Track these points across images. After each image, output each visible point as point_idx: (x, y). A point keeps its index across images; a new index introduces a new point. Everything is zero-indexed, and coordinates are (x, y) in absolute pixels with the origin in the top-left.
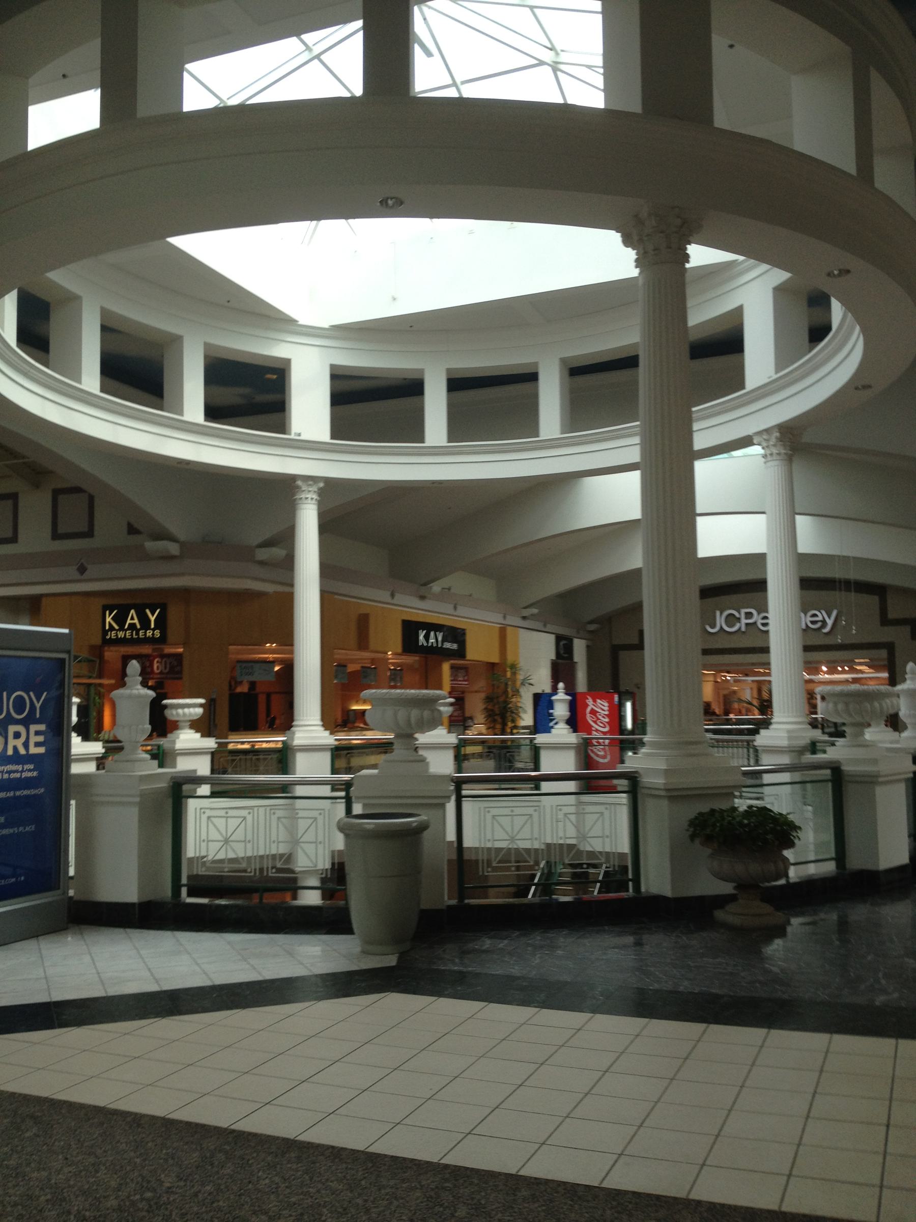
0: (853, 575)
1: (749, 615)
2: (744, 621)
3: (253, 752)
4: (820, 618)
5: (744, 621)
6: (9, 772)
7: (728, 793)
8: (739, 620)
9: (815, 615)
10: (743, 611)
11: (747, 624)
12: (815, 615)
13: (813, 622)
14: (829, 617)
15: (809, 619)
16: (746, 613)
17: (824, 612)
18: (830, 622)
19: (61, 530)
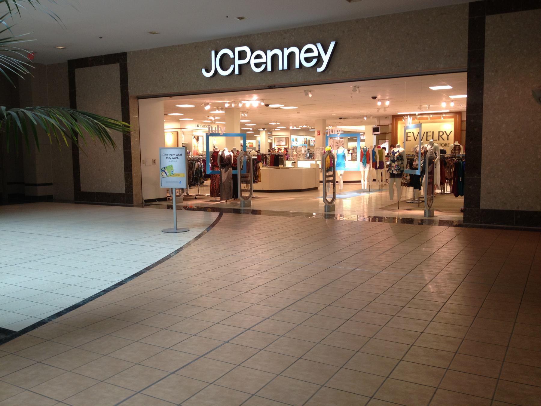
0: (135, 180)
1: (242, 55)
2: (238, 62)
3: (393, 190)
4: (315, 54)
5: (238, 62)
6: (216, 201)
7: (462, 121)
8: (233, 61)
9: (309, 51)
10: (237, 49)
11: (240, 66)
12: (309, 51)
13: (308, 60)
14: (326, 53)
15: (304, 55)
16: (240, 53)
17: (319, 45)
18: (326, 58)
19: (115, 68)
